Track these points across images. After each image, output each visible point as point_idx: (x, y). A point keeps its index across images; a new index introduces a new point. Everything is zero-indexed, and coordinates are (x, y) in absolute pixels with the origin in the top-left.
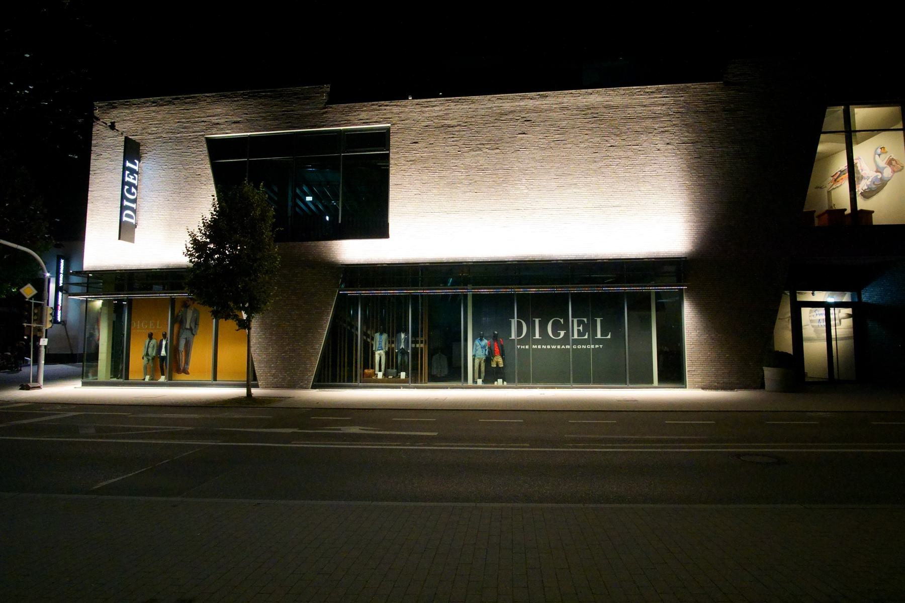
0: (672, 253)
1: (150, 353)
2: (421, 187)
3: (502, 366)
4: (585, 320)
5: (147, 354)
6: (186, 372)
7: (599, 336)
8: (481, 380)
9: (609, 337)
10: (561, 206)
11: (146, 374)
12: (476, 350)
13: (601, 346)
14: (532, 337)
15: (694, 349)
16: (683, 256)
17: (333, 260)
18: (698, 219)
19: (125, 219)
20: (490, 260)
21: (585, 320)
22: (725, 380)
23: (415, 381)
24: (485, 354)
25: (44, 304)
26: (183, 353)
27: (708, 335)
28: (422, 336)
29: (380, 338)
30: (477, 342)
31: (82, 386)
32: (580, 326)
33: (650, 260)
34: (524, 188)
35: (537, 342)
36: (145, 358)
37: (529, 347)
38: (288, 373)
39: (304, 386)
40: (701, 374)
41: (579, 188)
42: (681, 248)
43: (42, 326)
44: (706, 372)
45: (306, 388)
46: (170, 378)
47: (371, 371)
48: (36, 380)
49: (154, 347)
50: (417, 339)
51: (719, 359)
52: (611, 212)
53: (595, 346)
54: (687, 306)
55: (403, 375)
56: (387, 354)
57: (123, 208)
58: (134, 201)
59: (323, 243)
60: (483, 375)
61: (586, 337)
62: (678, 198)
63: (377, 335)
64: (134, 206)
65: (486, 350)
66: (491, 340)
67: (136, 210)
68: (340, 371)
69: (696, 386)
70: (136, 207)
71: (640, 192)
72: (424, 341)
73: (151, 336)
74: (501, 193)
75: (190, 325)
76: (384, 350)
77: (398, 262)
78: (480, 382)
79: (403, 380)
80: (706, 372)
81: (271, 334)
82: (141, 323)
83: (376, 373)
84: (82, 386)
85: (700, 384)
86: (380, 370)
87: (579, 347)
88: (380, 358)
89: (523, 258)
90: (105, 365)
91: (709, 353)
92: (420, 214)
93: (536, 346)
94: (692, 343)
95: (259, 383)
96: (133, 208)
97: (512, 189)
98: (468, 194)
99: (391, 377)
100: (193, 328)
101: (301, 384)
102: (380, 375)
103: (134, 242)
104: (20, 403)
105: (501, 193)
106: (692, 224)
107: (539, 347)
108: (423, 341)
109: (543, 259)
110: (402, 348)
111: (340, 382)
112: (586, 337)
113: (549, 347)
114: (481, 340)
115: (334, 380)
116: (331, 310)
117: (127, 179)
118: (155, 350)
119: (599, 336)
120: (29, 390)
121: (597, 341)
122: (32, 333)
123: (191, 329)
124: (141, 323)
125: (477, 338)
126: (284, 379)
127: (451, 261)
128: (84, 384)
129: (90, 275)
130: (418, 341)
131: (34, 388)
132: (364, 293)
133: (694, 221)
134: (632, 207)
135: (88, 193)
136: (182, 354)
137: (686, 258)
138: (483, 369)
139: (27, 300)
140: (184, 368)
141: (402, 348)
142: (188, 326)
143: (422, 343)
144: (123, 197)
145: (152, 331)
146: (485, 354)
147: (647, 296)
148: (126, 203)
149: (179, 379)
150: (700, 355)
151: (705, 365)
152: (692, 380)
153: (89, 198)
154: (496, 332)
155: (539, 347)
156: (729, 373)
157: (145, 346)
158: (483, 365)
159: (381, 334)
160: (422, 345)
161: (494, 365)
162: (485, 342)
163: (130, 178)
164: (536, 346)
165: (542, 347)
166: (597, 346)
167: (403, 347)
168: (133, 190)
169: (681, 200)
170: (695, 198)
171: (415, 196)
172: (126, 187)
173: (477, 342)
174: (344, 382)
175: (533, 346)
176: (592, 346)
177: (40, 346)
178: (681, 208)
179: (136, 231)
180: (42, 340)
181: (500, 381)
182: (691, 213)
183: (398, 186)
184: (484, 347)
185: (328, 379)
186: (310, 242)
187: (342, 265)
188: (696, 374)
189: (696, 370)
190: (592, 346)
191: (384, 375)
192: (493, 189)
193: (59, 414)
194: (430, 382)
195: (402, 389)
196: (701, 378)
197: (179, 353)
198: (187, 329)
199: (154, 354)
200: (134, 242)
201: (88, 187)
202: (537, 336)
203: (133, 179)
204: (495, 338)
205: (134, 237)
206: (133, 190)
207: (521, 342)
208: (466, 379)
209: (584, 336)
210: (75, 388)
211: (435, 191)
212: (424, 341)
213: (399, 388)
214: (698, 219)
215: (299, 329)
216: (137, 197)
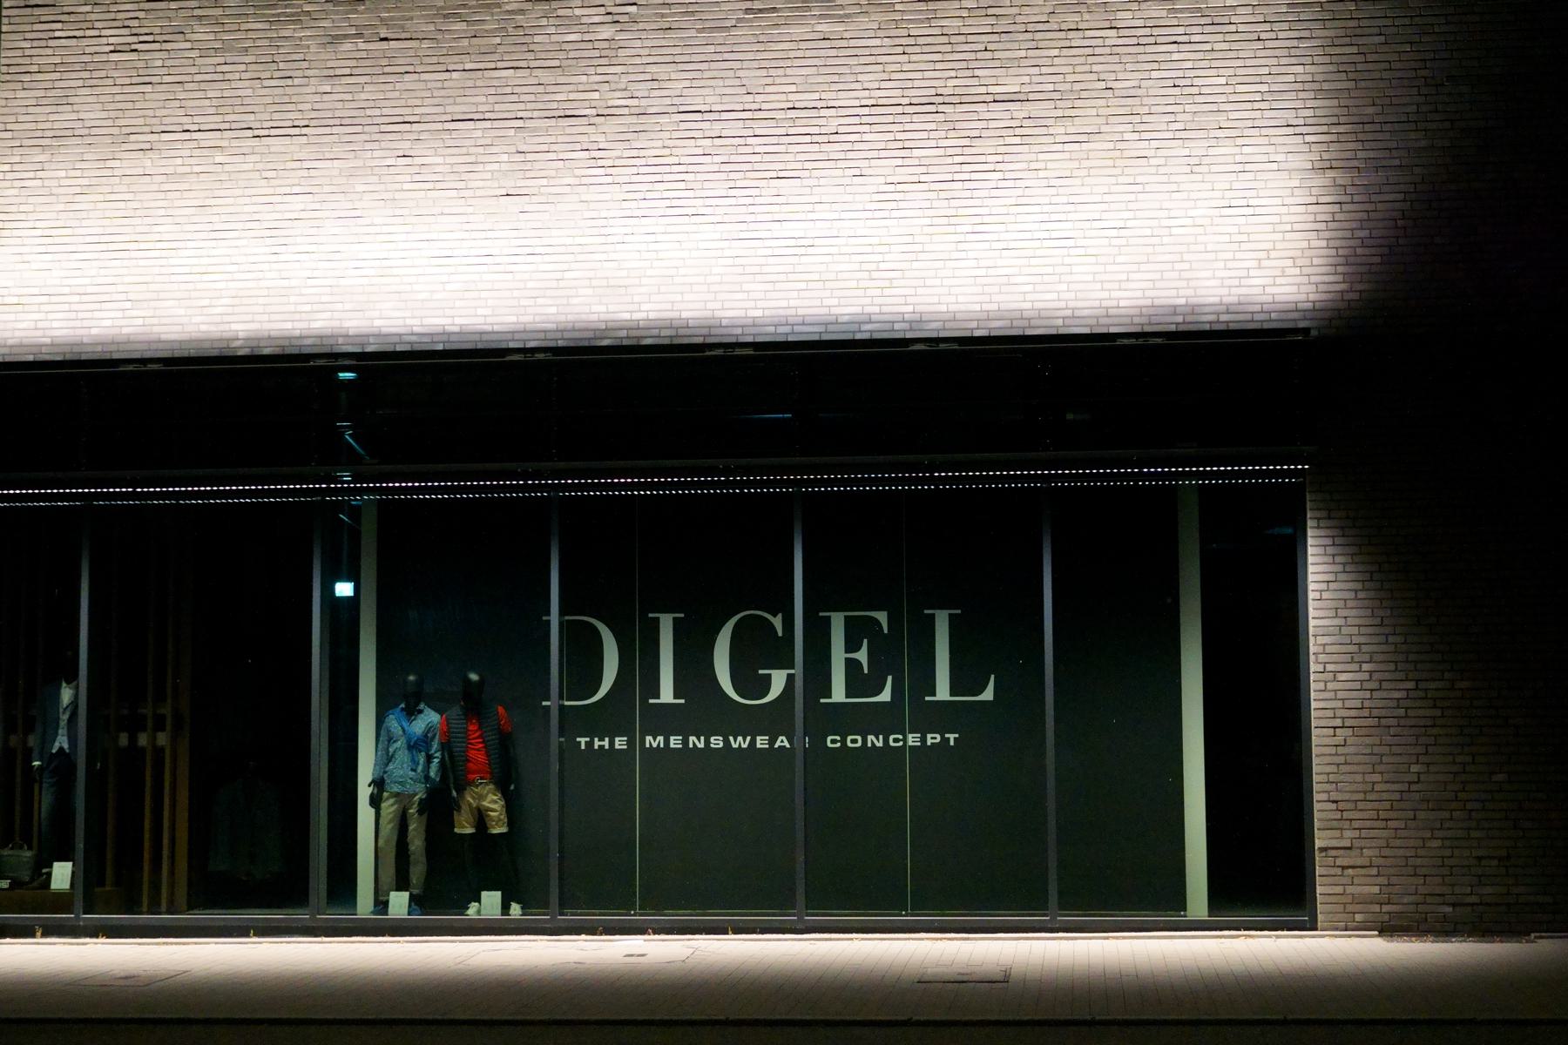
0: (623, 333)
2: (141, 15)
3: (504, 830)
4: (882, 617)
7: (943, 693)
8: (406, 895)
9: (988, 695)
10: (759, 98)
12: (390, 759)
13: (952, 737)
14: (644, 700)
15: (1351, 750)
16: (1302, 325)
18: (1372, 154)
20: (440, 347)
21: (882, 617)
22: (1489, 890)
24: (427, 778)
27: (1411, 685)
30: (394, 723)
32: (857, 649)
33: (1141, 341)
34: (596, 19)
35: (664, 719)
37: (631, 743)
40: (1376, 861)
41: (842, 19)
42: (1294, 289)
44: (1401, 852)
51: (1461, 795)
52: (983, 124)
53: (923, 740)
54: (1320, 550)
55: (61, 874)
60: (417, 872)
61: (885, 696)
62: (1284, 61)
65: (429, 758)
66: (455, 711)
69: (1358, 917)
71: (1113, 33)
72: (169, 721)
74: (498, 40)
78: (399, 903)
79: (60, 895)
80: (1401, 852)
85: (1377, 908)
87: (854, 741)
89: (590, 335)
91: (1414, 768)
92: (133, 138)
93: (661, 739)
94: (1338, 722)
97: (544, 22)
98: (347, 46)
105: (498, 40)
106: (1342, 178)
107: (675, 742)
108: (163, 717)
109: (677, 341)
110: (61, 749)
112: (885, 696)
113: (717, 742)
114: (412, 712)
119: (943, 693)
121: (941, 716)
125: (397, 705)
127: (266, 351)
129: (343, 375)
132: (572, 485)
133: (1356, 163)
134: (1078, 103)
137: (1306, 331)
138: (417, 843)
141: (61, 749)
143: (159, 725)
146: (427, 778)
147: (1166, 499)
150: (1377, 778)
151: (1401, 824)
152: (1339, 889)
154: (474, 677)
155: (675, 742)
156: (1508, 857)
158: (416, 828)
160: (162, 739)
161: (464, 827)
162: (429, 718)
164: (661, 739)
165: (707, 742)
166: (933, 739)
167: (66, 746)
169: (1300, 69)
170: (1360, 58)
171: (115, 57)
173: (394, 723)
175: (649, 738)
176: (913, 740)
178: (1299, 104)
181: (491, 901)
182: (1341, 129)
183: (37, 11)
184: (414, 746)
188: (1359, 862)
189: (1357, 843)
190: (913, 740)
192: (463, 26)
194: (192, 909)
196: (1380, 880)
202: (667, 695)
204: (473, 703)
207: (597, 720)
208: (342, 885)
209: (879, 691)
211: (202, 33)
212: (169, 721)
214: (1372, 154)
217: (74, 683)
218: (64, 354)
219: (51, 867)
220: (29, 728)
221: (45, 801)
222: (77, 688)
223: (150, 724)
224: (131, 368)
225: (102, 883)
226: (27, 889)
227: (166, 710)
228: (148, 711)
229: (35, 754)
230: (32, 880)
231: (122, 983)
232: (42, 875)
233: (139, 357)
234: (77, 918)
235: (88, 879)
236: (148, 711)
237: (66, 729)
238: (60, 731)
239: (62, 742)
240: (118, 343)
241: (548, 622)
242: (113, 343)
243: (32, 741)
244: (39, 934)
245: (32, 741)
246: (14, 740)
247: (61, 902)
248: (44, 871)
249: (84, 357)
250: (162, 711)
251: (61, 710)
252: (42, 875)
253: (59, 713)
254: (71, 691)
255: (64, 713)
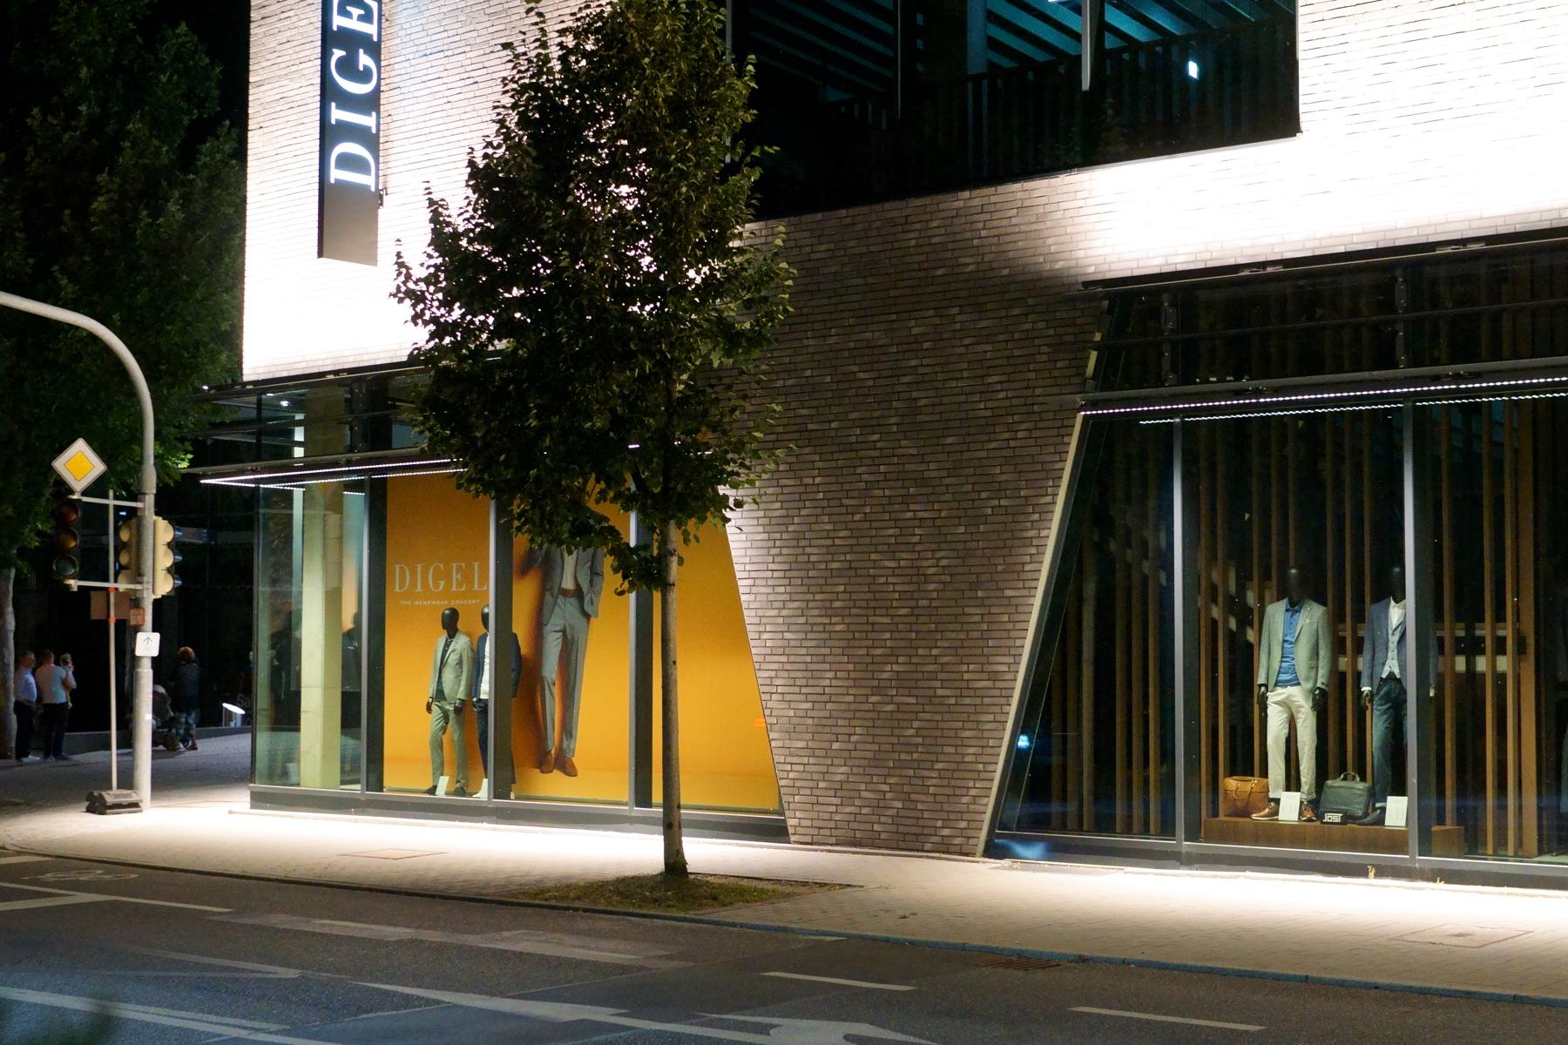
1: (447, 691)
5: (440, 695)
6: (565, 765)
11: (439, 770)
17: (1059, 265)
19: (336, 174)
23: (1472, 842)
25: (143, 509)
26: (556, 690)
28: (1500, 617)
29: (1289, 625)
31: (253, 807)
36: (434, 708)
38: (892, 780)
39: (957, 841)
43: (139, 587)
45: (965, 853)
46: (500, 790)
47: (1253, 783)
48: (127, 781)
49: (460, 663)
50: (1478, 633)
56: (1321, 703)
57: (329, 134)
58: (371, 103)
59: (1016, 189)
63: (1276, 612)
64: (368, 121)
67: (377, 136)
68: (1502, 808)
70: (378, 125)
72: (1488, 642)
73: (451, 624)
75: (575, 578)
76: (1309, 685)
77: (1342, 249)
81: (828, 611)
82: (425, 572)
83: (1272, 795)
84: (253, 807)
86: (1292, 783)
88: (1292, 724)
90: (320, 732)
95: (791, 822)
96: (367, 129)
99: (1336, 818)
100: (585, 586)
101: (946, 832)
102: (1290, 807)
103: (376, 265)
104: (19, 853)
110: (1391, 675)
111: (1129, 830)
115: (1104, 824)
116: (1055, 495)
117: (338, 21)
118: (464, 676)
120: (102, 813)
122: (112, 613)
123: (578, 593)
124: (425, 572)
126: (879, 806)
128: (259, 800)
130: (1483, 639)
131: (118, 807)
135: (247, 94)
136: (552, 694)
139: (75, 497)
140: (561, 750)
141: (1391, 675)
142: (568, 584)
143: (1500, 647)
144: (328, 92)
145: (455, 603)
148: (337, 114)
149: (553, 795)
153: (250, 111)
157: (435, 666)
159: (1294, 607)
160: (1504, 663)
163: (349, 15)
167: (1397, 671)
168: (364, 60)
172: (338, 53)
174: (1145, 831)
177: (140, 658)
179: (380, 218)
180: (140, 637)
185: (1520, 843)
186: (966, 194)
187: (1087, 284)
191: (1315, 806)
193: (62, 895)
194: (1549, 852)
195: (1372, 880)
197: (543, 683)
198: (565, 593)
199: (461, 694)
200: (376, 265)
201: (247, 72)
203: (361, 18)
205: (376, 242)
206: (364, 60)
210: (231, 812)
212: (1488, 642)
213: (1357, 871)
215: (931, 587)
216: (378, 85)
217: (1402, 603)
218: (1378, 242)
219: (1385, 801)
220: (1359, 649)
221: (1377, 728)
222: (1405, 607)
223: (107, 1003)
224: (1449, 250)
225: (1441, 820)
226: (1359, 824)
227: (1507, 632)
228: (1484, 631)
229: (1365, 679)
230: (1366, 814)
231: (1455, 941)
232: (1375, 809)
233: (1459, 237)
234: (1413, 858)
235: (1426, 817)
236: (1484, 631)
237: (1396, 652)
238: (1390, 654)
239: (1391, 666)
240: (1436, 225)
241: (156, 681)
242: (1429, 225)
243: (1362, 664)
244: (1372, 874)
245: (1362, 664)
246: (1344, 663)
247: (1395, 842)
248: (1378, 805)
249: (1398, 243)
250: (1501, 633)
251: (1390, 632)
252: (1375, 809)
253: (1387, 634)
254: (1401, 611)
255: (1393, 634)
